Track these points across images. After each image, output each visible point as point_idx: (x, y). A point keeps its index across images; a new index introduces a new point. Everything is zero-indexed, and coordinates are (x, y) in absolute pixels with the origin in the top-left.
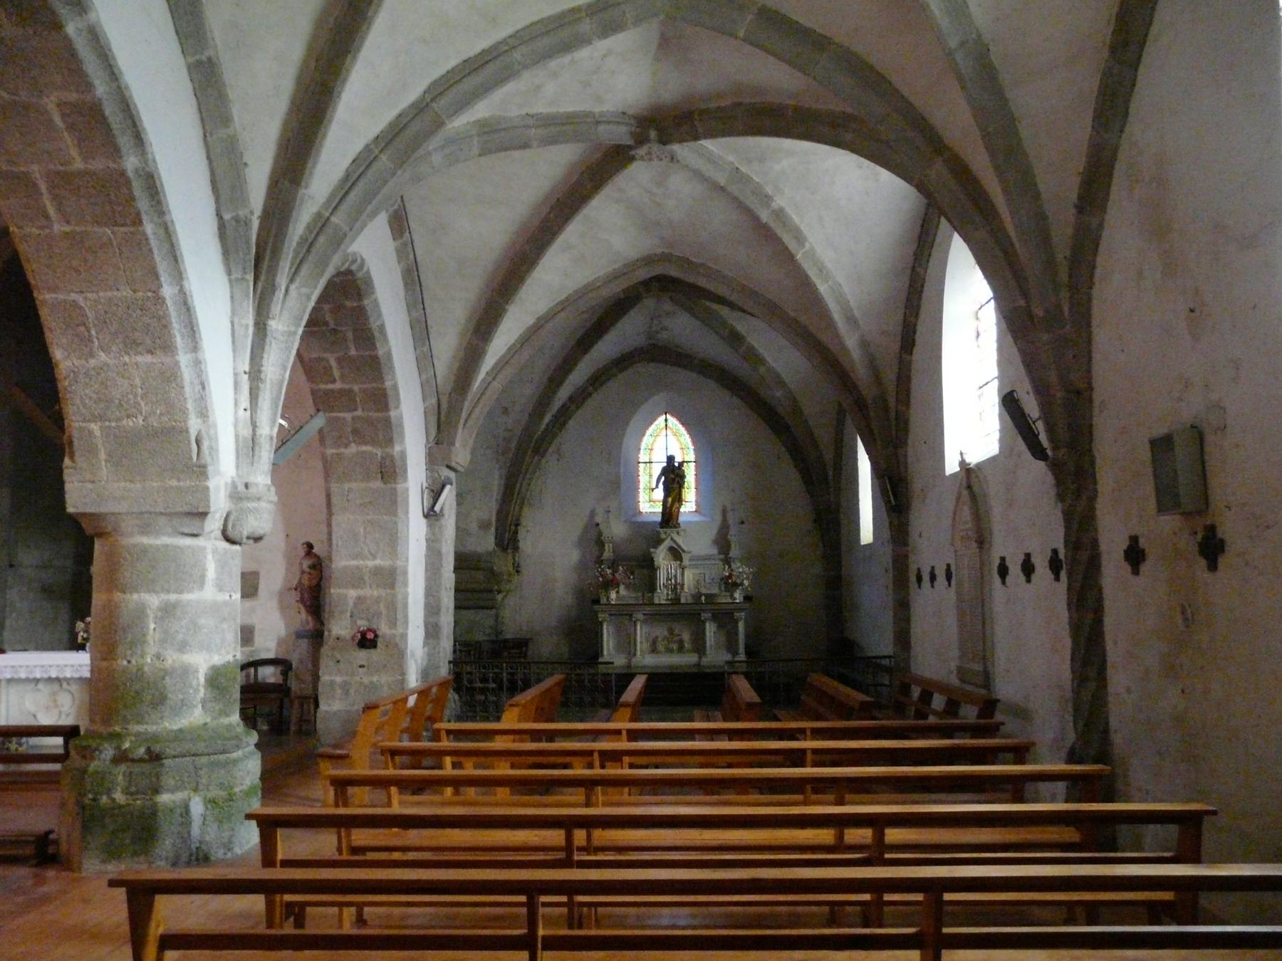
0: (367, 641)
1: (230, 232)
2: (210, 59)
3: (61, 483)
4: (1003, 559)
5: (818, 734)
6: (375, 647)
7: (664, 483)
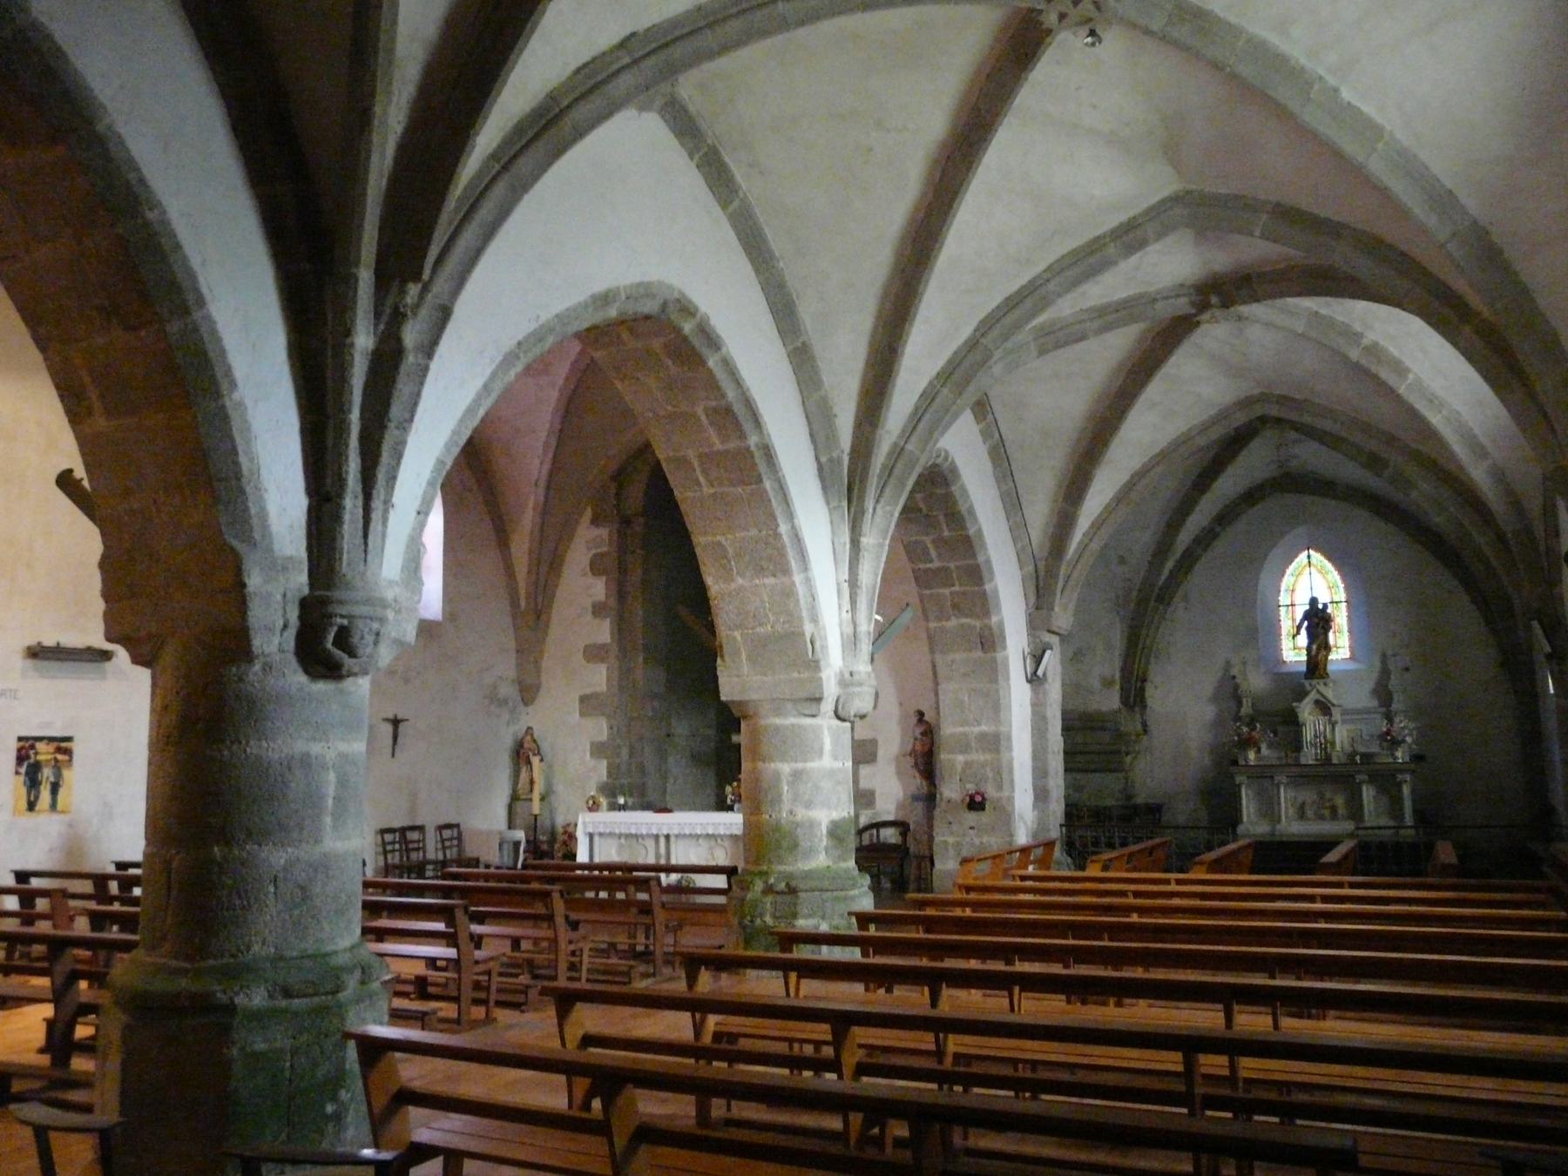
0: (976, 804)
1: (826, 469)
2: (804, 343)
3: (716, 678)
5: (1352, 885)
6: (983, 809)
7: (1308, 629)
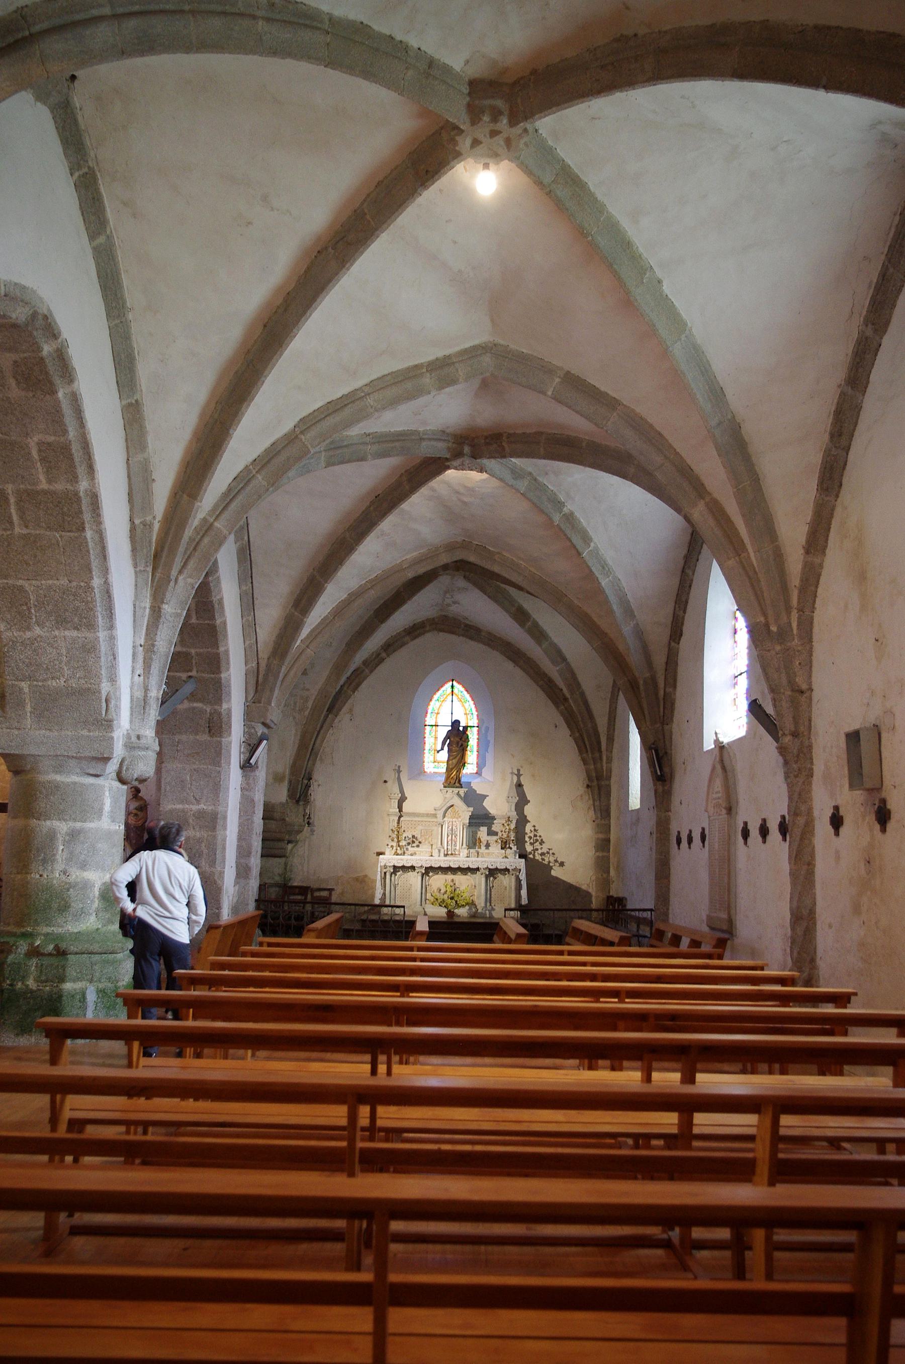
1: (139, 531)
2: (137, 401)
4: (746, 823)
